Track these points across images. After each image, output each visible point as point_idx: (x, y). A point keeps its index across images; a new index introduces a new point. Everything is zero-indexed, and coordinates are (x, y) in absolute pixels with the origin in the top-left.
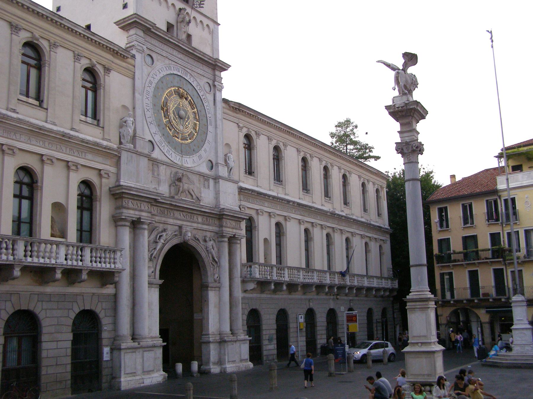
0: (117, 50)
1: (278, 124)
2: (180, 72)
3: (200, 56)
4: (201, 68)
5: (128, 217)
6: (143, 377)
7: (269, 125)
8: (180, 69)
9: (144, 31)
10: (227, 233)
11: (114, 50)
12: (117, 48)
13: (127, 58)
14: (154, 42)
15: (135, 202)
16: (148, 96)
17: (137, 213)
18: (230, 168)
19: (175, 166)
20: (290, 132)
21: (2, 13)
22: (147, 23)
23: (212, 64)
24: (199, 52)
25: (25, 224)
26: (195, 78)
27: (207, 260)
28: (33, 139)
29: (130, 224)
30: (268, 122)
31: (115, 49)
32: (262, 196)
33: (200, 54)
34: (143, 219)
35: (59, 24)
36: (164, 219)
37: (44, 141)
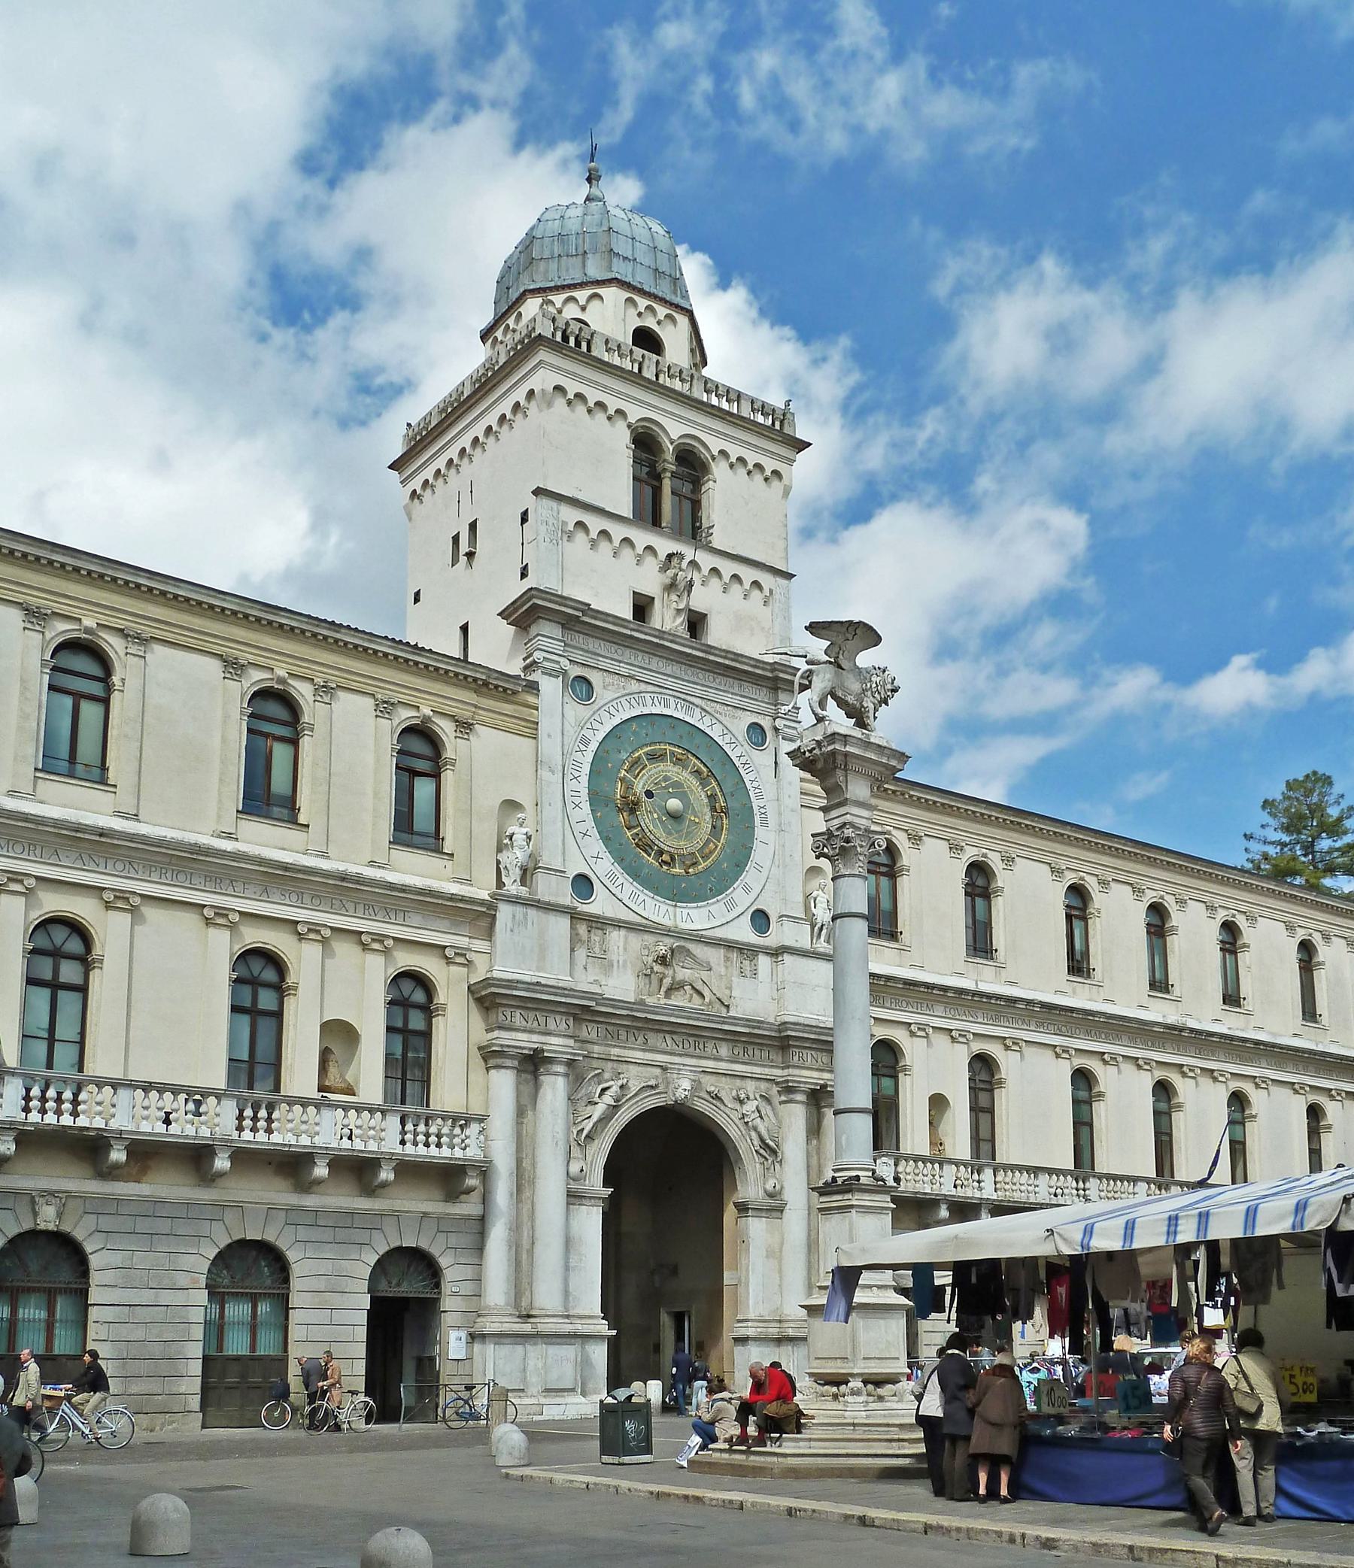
0: (484, 678)
1: (975, 806)
2: (673, 705)
3: (727, 662)
4: (736, 691)
5: (508, 1046)
6: (543, 1401)
7: (1031, 831)
8: (672, 699)
9: (563, 625)
10: (800, 1082)
11: (475, 680)
12: (482, 673)
13: (515, 693)
14: (593, 644)
15: (531, 1015)
16: (577, 774)
17: (535, 1038)
18: (819, 925)
19: (653, 928)
20: (1019, 824)
21: (5, 589)
22: (566, 606)
23: (768, 678)
24: (723, 654)
25: (985, 1143)
26: (717, 716)
27: (745, 1145)
28: (275, 890)
29: (519, 1062)
30: (943, 804)
31: (478, 676)
32: (922, 990)
33: (725, 658)
34: (549, 1051)
35: (331, 641)
36: (615, 1051)
37: (300, 895)
